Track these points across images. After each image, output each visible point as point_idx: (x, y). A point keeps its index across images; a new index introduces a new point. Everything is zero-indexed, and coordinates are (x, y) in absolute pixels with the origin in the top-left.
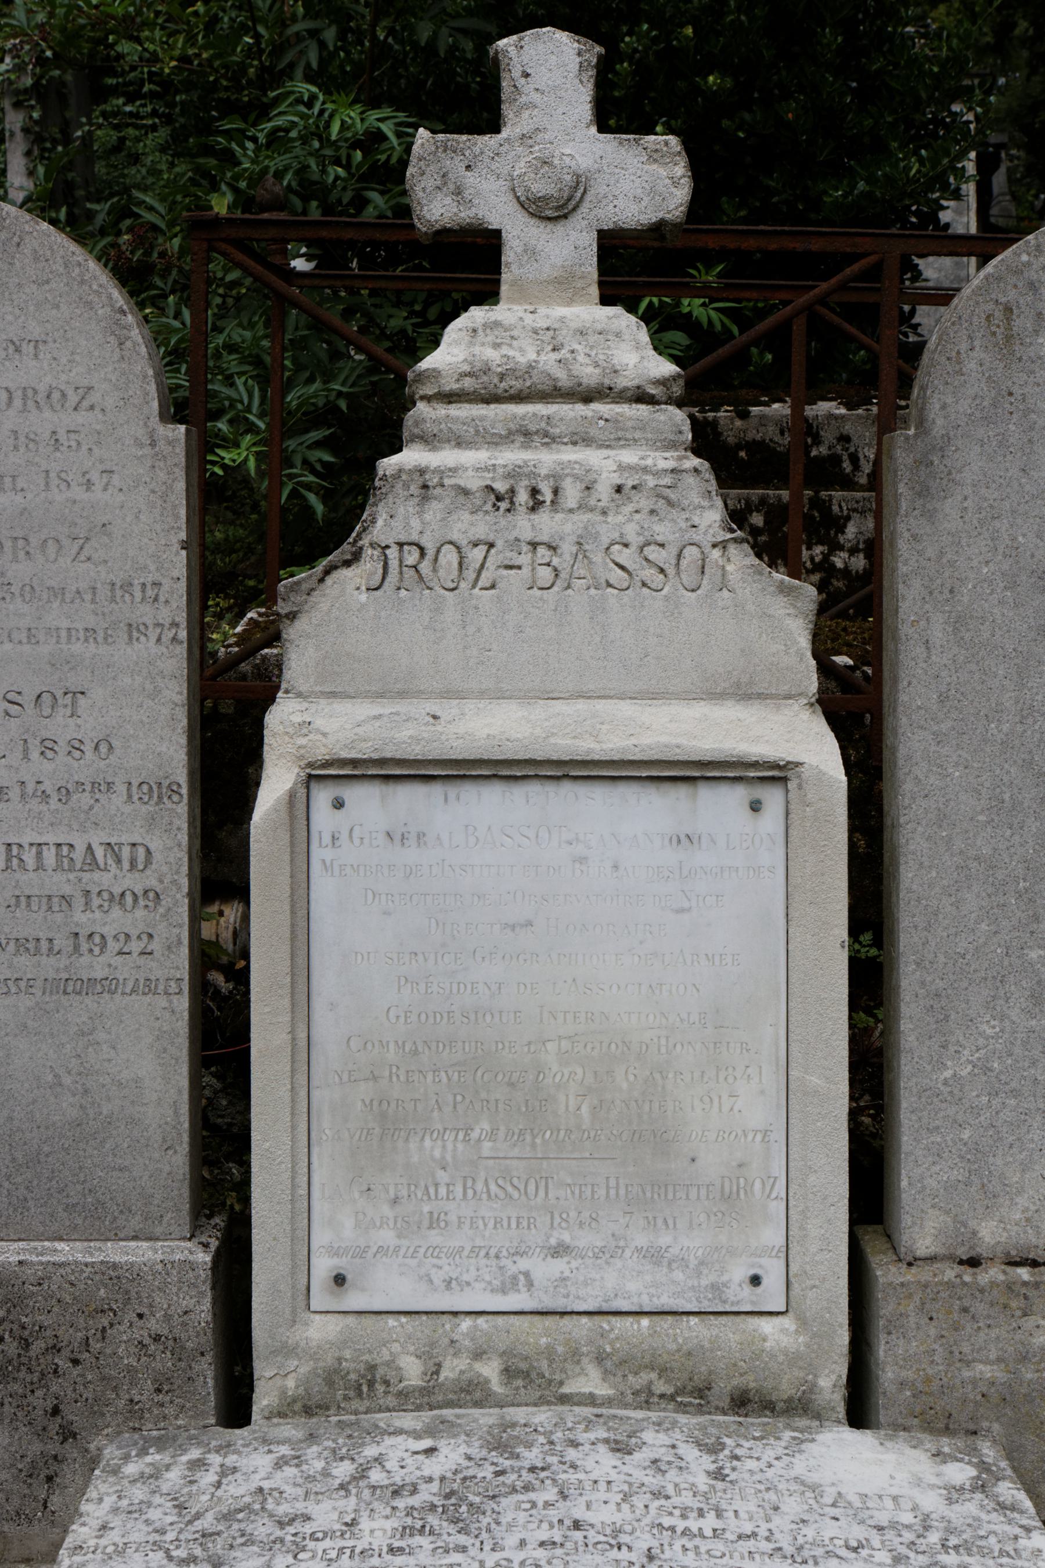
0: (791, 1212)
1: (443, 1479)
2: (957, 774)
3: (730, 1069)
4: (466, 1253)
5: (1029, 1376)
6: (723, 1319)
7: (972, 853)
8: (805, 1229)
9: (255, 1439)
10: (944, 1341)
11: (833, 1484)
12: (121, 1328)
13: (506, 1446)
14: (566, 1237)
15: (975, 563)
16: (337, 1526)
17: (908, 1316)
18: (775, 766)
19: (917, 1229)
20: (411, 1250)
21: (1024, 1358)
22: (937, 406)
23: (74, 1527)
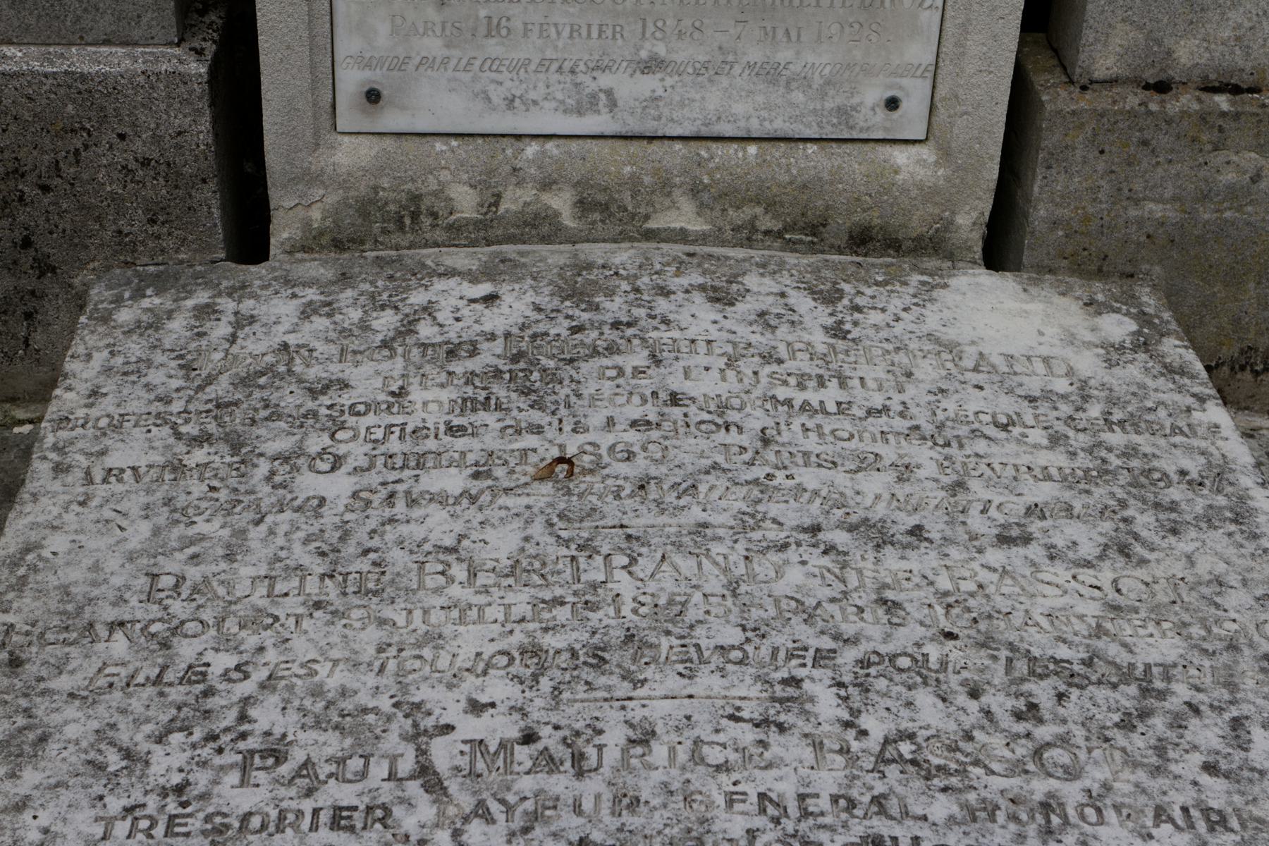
0: (947, 24)
1: (507, 335)
4: (532, 67)
5: (1206, 216)
6: (848, 148)
8: (962, 46)
9: (275, 279)
11: (973, 343)
12: (99, 151)
13: (582, 294)
14: (661, 50)
16: (382, 397)
17: (1074, 149)
19: (1099, 47)
20: (464, 62)
21: (1204, 197)
23: (58, 392)
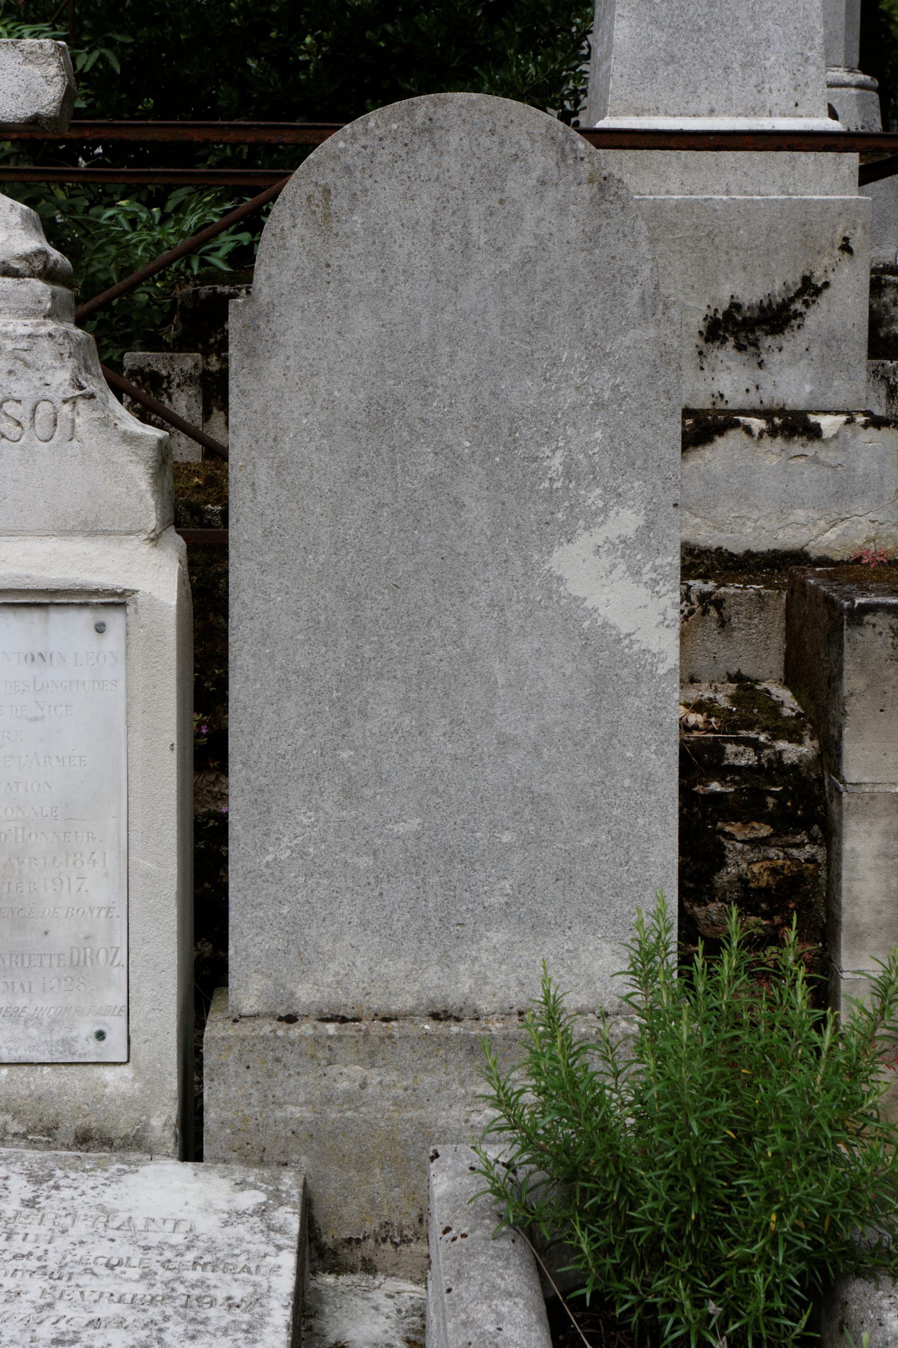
2: (279, 599)
3: (78, 856)
5: (333, 1116)
6: (73, 1069)
7: (291, 667)
10: (260, 1086)
15: (296, 415)
17: (228, 1066)
18: (114, 593)
19: (242, 991)
21: (328, 1101)
22: (263, 277)
